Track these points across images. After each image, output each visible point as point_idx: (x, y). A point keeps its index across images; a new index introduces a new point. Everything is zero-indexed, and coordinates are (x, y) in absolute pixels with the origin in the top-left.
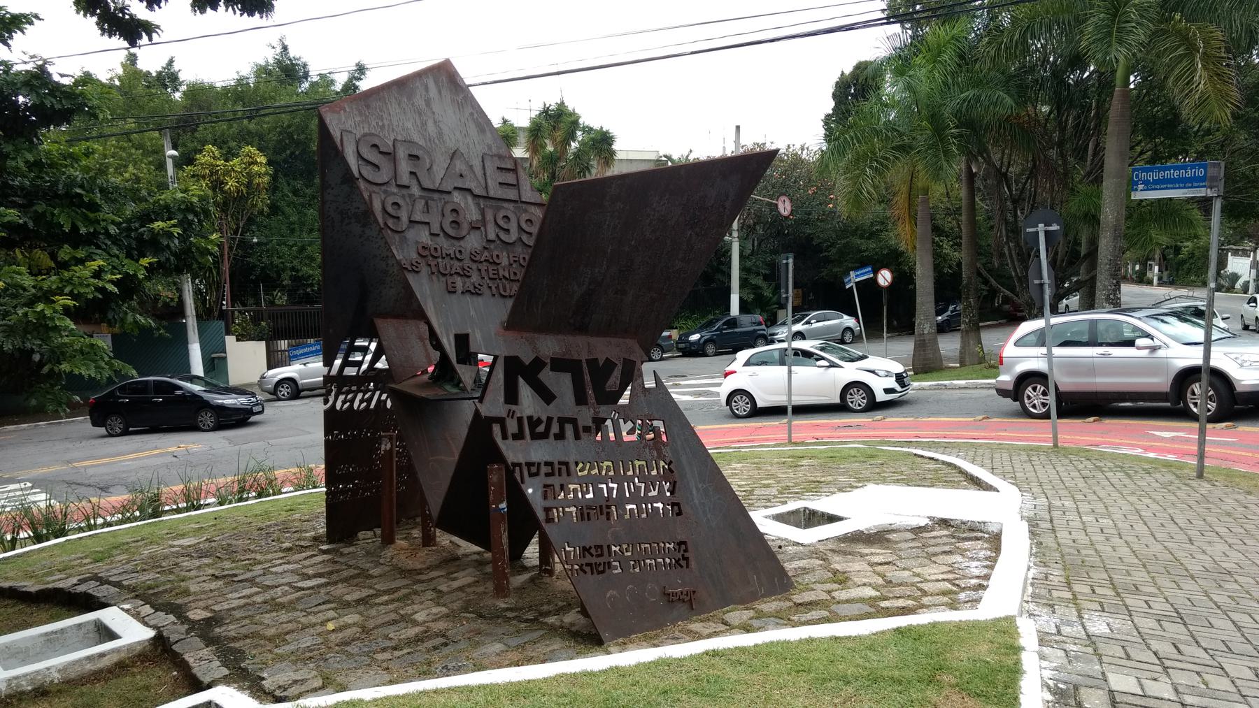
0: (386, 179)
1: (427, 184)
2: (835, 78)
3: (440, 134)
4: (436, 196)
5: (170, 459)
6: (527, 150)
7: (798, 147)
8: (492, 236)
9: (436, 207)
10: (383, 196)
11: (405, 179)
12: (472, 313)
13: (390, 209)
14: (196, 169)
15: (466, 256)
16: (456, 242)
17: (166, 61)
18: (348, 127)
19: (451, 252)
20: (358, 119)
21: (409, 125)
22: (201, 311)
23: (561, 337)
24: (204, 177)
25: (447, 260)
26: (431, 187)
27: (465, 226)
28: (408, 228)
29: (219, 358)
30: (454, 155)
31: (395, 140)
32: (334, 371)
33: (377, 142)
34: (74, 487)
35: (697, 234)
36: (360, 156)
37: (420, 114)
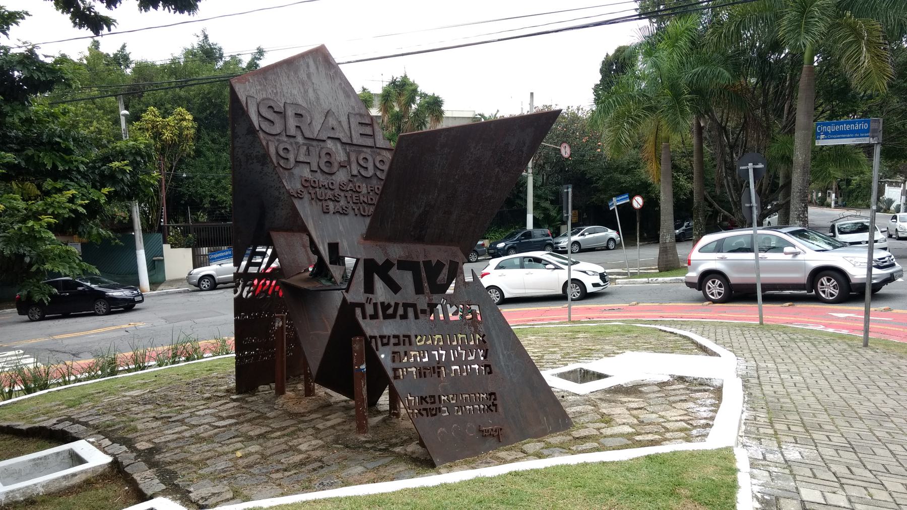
0: (279, 132)
1: (308, 135)
2: (602, 58)
3: (318, 99)
4: (315, 143)
6: (380, 110)
7: (575, 108)
8: (355, 172)
9: (314, 151)
11: (292, 131)
12: (341, 228)
13: (281, 153)
15: (336, 187)
16: (329, 177)
17: (121, 46)
18: (251, 93)
19: (326, 183)
20: (259, 88)
21: (295, 92)
22: (145, 226)
23: (404, 245)
24: (147, 130)
25: (323, 189)
26: (311, 137)
27: (336, 165)
28: (295, 166)
36: (260, 114)
37: (303, 84)
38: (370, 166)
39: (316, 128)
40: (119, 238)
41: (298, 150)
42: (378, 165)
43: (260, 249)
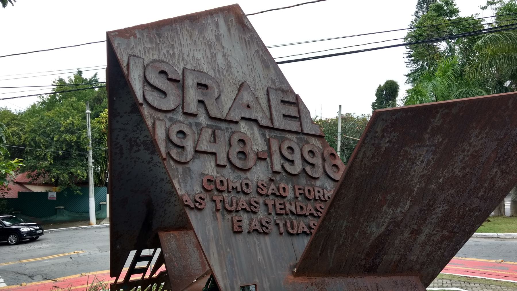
0: (173, 107)
1: (214, 113)
2: (377, 87)
3: (229, 66)
4: (223, 125)
5: (69, 259)
7: (366, 115)
8: (278, 168)
9: (223, 136)
10: (168, 124)
11: (192, 107)
12: (260, 257)
13: (174, 138)
14: (101, 120)
15: (252, 190)
16: (242, 174)
17: (94, 74)
18: (136, 52)
19: (238, 185)
20: (148, 45)
21: (199, 56)
22: (97, 182)
24: (103, 123)
25: (233, 194)
26: (219, 116)
27: (252, 157)
28: (194, 158)
29: (103, 204)
30: (241, 87)
31: (184, 69)
32: (121, 280)
33: (166, 68)
34: (17, 275)
35: (502, 172)
36: (146, 81)
37: (210, 47)
38: (297, 158)
39: (225, 105)
40: (79, 190)
41: (200, 135)
42: (307, 157)
43: (145, 252)
